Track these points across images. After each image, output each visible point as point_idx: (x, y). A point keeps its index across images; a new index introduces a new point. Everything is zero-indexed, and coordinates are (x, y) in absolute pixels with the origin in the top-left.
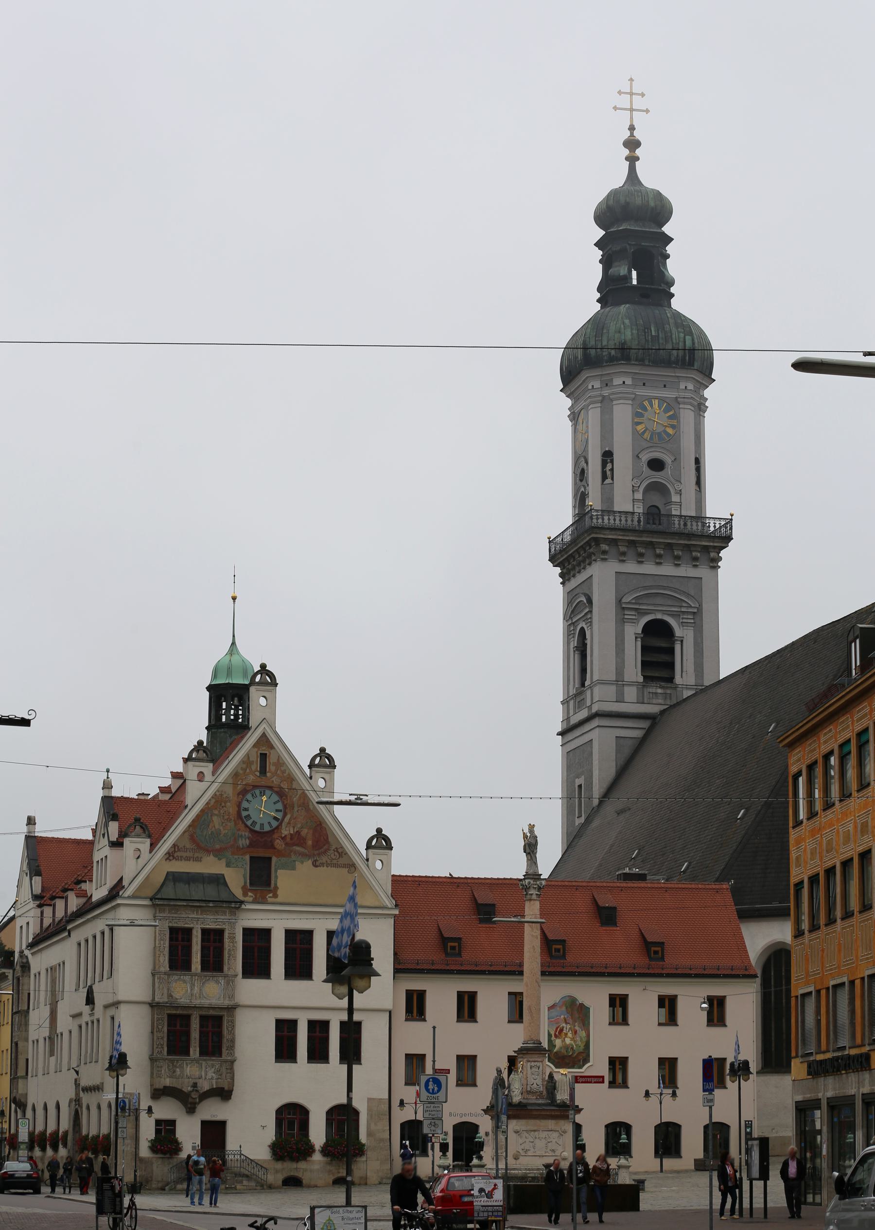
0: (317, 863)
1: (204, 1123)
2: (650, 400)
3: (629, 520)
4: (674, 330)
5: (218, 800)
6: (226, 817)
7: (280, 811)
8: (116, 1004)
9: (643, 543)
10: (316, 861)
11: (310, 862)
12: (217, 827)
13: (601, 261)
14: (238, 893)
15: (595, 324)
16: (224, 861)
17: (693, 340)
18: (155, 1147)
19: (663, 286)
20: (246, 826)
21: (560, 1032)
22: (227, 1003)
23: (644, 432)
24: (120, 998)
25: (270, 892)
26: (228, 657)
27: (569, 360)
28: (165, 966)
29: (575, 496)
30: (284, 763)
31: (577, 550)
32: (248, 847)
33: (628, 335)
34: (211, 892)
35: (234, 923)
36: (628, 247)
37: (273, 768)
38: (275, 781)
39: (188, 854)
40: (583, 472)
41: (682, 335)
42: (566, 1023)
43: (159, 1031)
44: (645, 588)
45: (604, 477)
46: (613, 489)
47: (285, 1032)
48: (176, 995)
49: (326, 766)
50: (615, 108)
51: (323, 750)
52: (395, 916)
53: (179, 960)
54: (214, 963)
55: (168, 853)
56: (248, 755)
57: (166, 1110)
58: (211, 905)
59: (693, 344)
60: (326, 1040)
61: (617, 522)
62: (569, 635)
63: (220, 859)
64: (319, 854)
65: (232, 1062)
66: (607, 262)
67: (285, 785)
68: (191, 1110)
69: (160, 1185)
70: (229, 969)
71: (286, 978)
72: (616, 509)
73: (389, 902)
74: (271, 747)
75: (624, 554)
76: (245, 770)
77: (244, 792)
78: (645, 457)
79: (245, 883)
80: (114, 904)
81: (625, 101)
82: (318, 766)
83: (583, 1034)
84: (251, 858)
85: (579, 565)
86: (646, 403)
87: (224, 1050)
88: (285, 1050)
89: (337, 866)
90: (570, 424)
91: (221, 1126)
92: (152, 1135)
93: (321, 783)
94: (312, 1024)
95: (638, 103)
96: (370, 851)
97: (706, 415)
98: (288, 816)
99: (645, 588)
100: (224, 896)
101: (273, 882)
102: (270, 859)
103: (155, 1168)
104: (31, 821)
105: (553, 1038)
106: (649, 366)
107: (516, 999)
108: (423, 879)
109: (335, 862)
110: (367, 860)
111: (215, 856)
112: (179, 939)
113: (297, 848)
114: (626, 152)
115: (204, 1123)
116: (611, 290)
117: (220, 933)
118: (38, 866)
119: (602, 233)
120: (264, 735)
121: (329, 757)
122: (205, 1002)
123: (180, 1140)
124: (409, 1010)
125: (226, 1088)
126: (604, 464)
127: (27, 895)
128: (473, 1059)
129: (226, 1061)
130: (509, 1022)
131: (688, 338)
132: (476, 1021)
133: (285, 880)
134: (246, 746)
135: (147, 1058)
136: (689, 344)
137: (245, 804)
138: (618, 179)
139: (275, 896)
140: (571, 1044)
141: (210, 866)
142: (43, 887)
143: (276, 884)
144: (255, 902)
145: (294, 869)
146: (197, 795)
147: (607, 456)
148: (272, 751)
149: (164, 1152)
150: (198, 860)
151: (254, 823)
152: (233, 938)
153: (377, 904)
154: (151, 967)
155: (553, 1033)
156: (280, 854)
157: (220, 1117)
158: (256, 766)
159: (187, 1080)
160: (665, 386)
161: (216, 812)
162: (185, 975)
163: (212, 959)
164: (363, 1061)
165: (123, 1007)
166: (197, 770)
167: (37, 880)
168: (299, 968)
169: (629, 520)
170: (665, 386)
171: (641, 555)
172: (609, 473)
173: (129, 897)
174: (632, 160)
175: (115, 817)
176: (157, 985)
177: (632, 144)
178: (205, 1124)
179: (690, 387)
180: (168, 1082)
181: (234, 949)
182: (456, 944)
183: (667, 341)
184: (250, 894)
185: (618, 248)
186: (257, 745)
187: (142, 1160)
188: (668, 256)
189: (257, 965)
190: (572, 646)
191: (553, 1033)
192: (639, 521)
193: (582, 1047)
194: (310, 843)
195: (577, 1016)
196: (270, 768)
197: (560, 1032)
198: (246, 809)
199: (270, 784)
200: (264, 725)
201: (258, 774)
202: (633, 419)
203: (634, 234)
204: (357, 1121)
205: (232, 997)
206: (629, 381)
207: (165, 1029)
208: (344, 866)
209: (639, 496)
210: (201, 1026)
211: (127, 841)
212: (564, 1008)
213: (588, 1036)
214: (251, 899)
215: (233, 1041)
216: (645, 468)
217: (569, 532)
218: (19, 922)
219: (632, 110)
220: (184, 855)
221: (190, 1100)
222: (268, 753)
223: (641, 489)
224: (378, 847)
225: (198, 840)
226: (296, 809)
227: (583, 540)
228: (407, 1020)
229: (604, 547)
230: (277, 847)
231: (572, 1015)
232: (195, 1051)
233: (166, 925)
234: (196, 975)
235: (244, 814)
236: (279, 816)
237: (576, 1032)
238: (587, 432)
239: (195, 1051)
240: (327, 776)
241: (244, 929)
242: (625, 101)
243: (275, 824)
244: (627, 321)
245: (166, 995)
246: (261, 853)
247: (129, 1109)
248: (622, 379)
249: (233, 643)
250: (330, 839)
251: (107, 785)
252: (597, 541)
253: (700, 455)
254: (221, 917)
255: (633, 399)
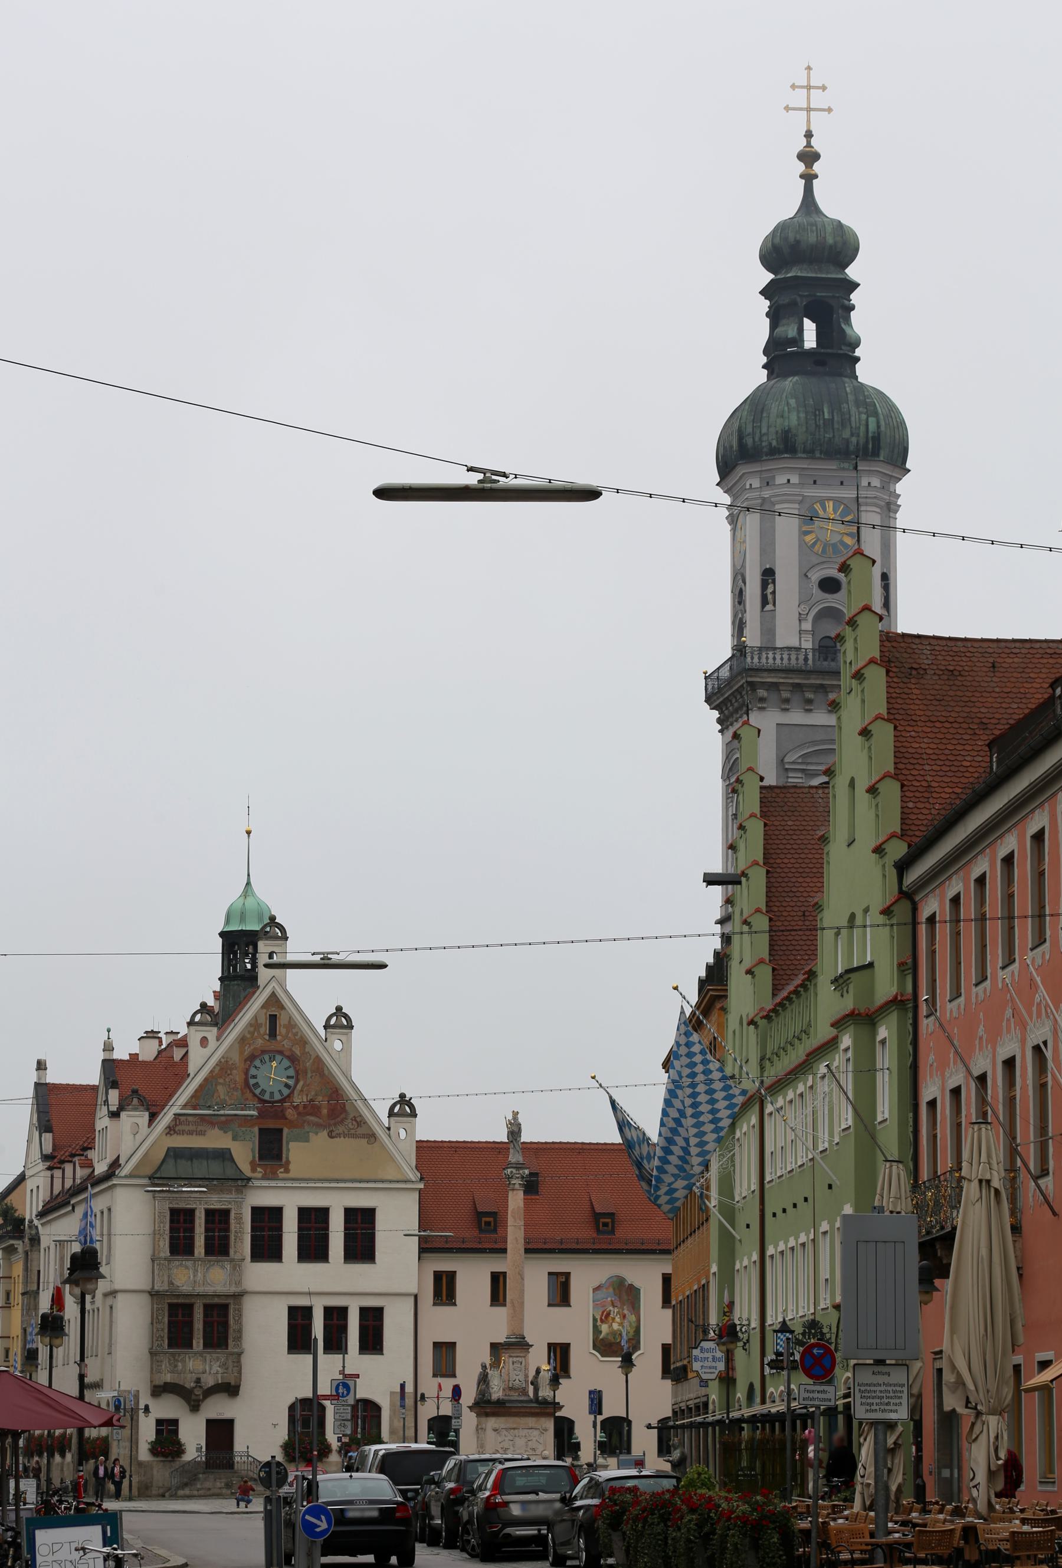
0: (334, 1134)
1: (209, 1422)
2: (822, 502)
3: (793, 657)
4: (853, 410)
5: (223, 1068)
6: (232, 1086)
7: (292, 1077)
8: (113, 1293)
9: (811, 686)
10: (331, 1131)
11: (325, 1133)
12: (222, 1097)
13: (768, 315)
14: (246, 1169)
15: (755, 406)
16: (230, 1134)
17: (878, 422)
18: (156, 1449)
19: (845, 349)
20: (255, 1095)
21: (606, 1317)
22: (233, 1289)
23: (815, 544)
24: (117, 1287)
25: (281, 1166)
26: (242, 900)
27: (725, 448)
28: (165, 1252)
29: (733, 623)
30: (296, 1025)
31: (732, 694)
32: (258, 1117)
33: (793, 420)
34: (216, 1168)
35: (241, 1203)
36: (799, 299)
37: (283, 1031)
38: (286, 1044)
39: (191, 1128)
40: (741, 592)
41: (864, 417)
42: (614, 1306)
43: (159, 1322)
44: (814, 743)
45: (764, 602)
46: (774, 618)
47: (299, 1319)
48: (177, 1283)
49: (343, 1027)
50: (787, 108)
51: (339, 1009)
52: (420, 1190)
53: (180, 1245)
54: (219, 1246)
55: (169, 1127)
56: (256, 1017)
57: (168, 1408)
58: (215, 1182)
59: (879, 427)
60: (344, 1328)
61: (778, 661)
62: (727, 798)
63: (225, 1132)
64: (335, 1124)
65: (240, 1354)
66: (775, 316)
67: (297, 1051)
68: (195, 1408)
69: (161, 1491)
70: (235, 1252)
71: (299, 1261)
72: (779, 644)
73: (413, 1175)
74: (282, 1007)
75: (787, 701)
76: (252, 1033)
77: (252, 1058)
78: (816, 576)
79: (254, 1157)
80: (110, 1183)
81: (799, 98)
82: (334, 1027)
83: (633, 1318)
84: (260, 1130)
85: (736, 711)
86: (817, 507)
87: (230, 1342)
88: (299, 1339)
89: (355, 1136)
90: (729, 527)
91: (229, 1424)
92: (152, 1437)
93: (338, 1045)
94: (364, 1311)
95: (818, 99)
96: (392, 1119)
97: (898, 515)
98: (301, 1083)
99: (814, 743)
100: (230, 1173)
101: (284, 1156)
102: (281, 1131)
103: (155, 1473)
104: (41, 1066)
105: (599, 1323)
106: (820, 458)
107: (498, 1280)
108: (461, 1145)
109: (353, 1132)
110: (389, 1129)
111: (220, 1129)
112: (180, 1221)
113: (312, 1118)
114: (801, 167)
115: (209, 1422)
116: (780, 355)
117: (225, 1213)
118: (48, 1121)
119: (771, 276)
120: (273, 995)
121: (346, 1016)
122: (210, 1290)
123: (183, 1441)
124: (437, 1294)
125: (233, 1383)
126: (764, 585)
127: (36, 1155)
128: (452, 1345)
129: (232, 1354)
130: (550, 1305)
131: (872, 421)
132: (570, 1306)
133: (298, 1153)
134: (259, 999)
135: (147, 1351)
136: (872, 426)
137: (253, 1071)
138: (789, 207)
139: (287, 1171)
140: (619, 1330)
141: (215, 1140)
142: (54, 1145)
143: (287, 1158)
144: (265, 1178)
145: (307, 1140)
146: (202, 1059)
147: (768, 575)
148: (283, 1012)
149: (165, 1455)
150: (202, 1133)
151: (263, 1092)
152: (239, 1218)
153: (399, 1177)
154: (150, 1252)
155: (598, 1317)
156: (292, 1125)
157: (227, 1416)
158: (265, 1029)
159: (189, 1376)
160: (842, 483)
161: (221, 1081)
162: (187, 1260)
163: (217, 1242)
164: (385, 1351)
165: (120, 1296)
166: (200, 1035)
167: (48, 1137)
168: (313, 1249)
169: (793, 657)
170: (842, 483)
171: (809, 701)
172: (770, 597)
173: (126, 1177)
174: (809, 178)
175: (114, 1085)
176: (156, 1272)
177: (808, 157)
178: (211, 1423)
179: (876, 482)
180: (168, 1378)
181: (241, 1231)
182: (491, 1219)
183: (843, 424)
184: (259, 1169)
185: (787, 301)
186: (265, 1006)
187: (140, 1464)
188: (853, 308)
189: (267, 1249)
190: (730, 813)
191: (598, 1317)
192: (806, 659)
193: (632, 1333)
194: (325, 1111)
195: (626, 1297)
196: (281, 1030)
197: (606, 1317)
198: (254, 1077)
199: (279, 1049)
200: (273, 984)
201: (267, 1037)
202: (800, 527)
203: (809, 273)
204: (379, 1417)
205: (239, 1283)
206: (795, 479)
207: (166, 1320)
208: (363, 1136)
209: (807, 626)
210: (206, 1315)
211: (123, 1114)
212: (611, 1290)
213: (638, 1321)
214: (260, 1175)
215: (240, 1331)
216: (816, 590)
217: (727, 667)
218: (30, 1184)
219: (809, 110)
220: (186, 1128)
221: (193, 1397)
222: (277, 1017)
223: (810, 618)
224: (402, 1114)
225: (206, 1110)
226: (309, 1075)
227: (737, 682)
228: (435, 1304)
229: (762, 693)
230: (289, 1117)
231: (620, 1298)
232: (198, 1342)
233: (167, 1206)
234: (199, 1259)
235: (252, 1081)
236: (291, 1082)
237: (624, 1316)
238: (744, 542)
239: (198, 1342)
240: (343, 1038)
241: (252, 1208)
242: (799, 98)
243: (286, 1092)
244: (792, 402)
245: (166, 1283)
246: (271, 1124)
247: (125, 1409)
248: (787, 477)
249: (248, 884)
250: (347, 1107)
251: (108, 1047)
252: (753, 686)
253: (889, 568)
254: (226, 1197)
255: (800, 502)
